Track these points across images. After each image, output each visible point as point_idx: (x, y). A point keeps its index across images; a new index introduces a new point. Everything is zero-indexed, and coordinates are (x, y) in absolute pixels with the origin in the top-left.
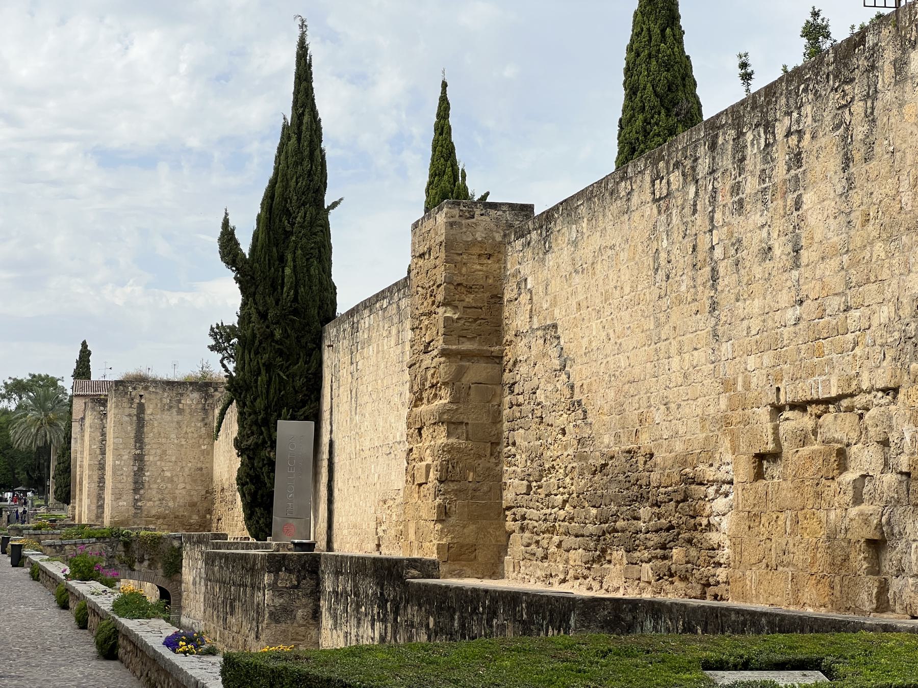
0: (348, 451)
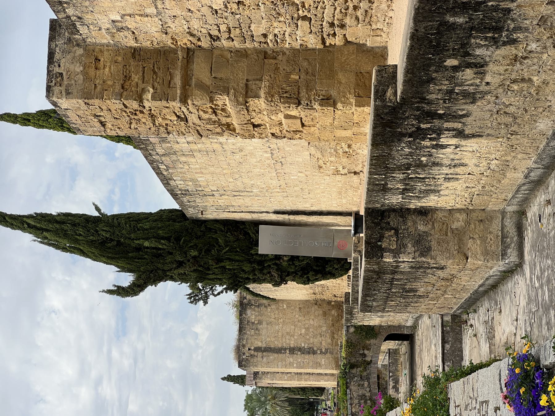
0: (281, 199)
